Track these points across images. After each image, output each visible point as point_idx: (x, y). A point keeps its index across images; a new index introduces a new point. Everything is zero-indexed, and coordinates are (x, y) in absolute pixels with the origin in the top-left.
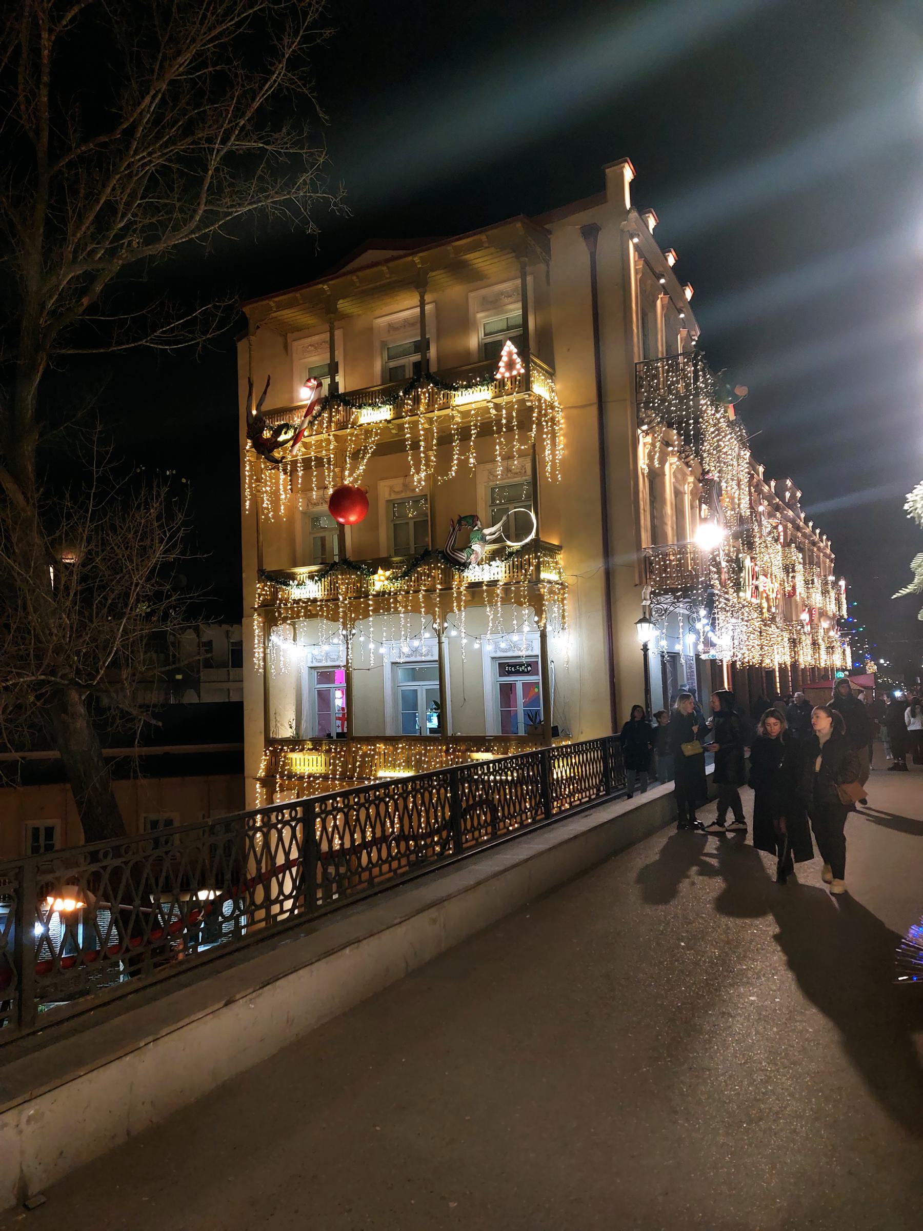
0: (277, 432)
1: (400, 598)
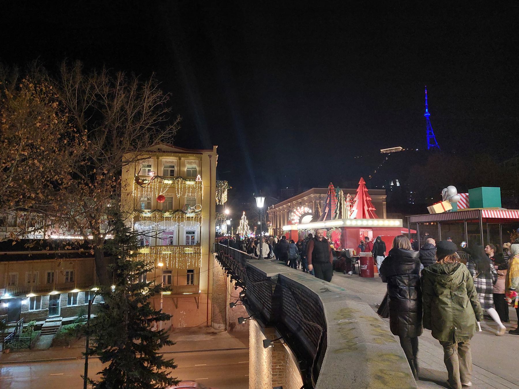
0: (144, 180)
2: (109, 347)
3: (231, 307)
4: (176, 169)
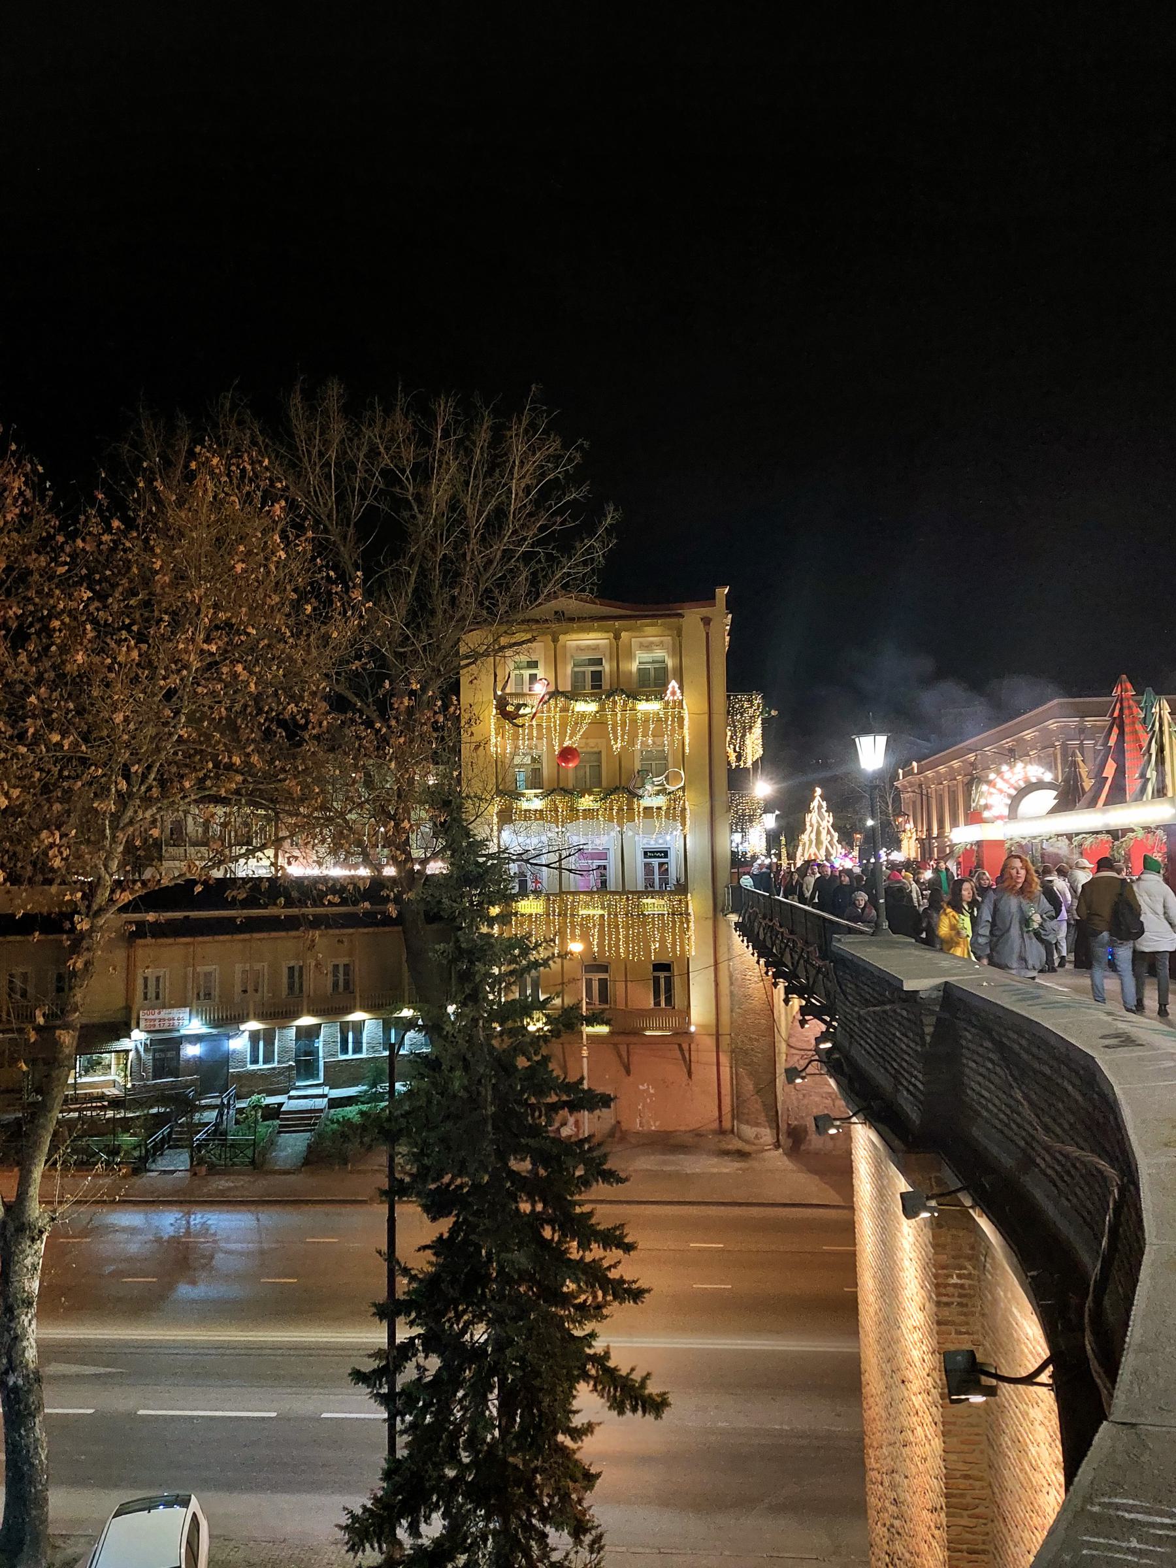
0: (519, 707)
1: (600, 813)
2: (447, 1179)
3: (790, 1080)
4: (607, 667)
